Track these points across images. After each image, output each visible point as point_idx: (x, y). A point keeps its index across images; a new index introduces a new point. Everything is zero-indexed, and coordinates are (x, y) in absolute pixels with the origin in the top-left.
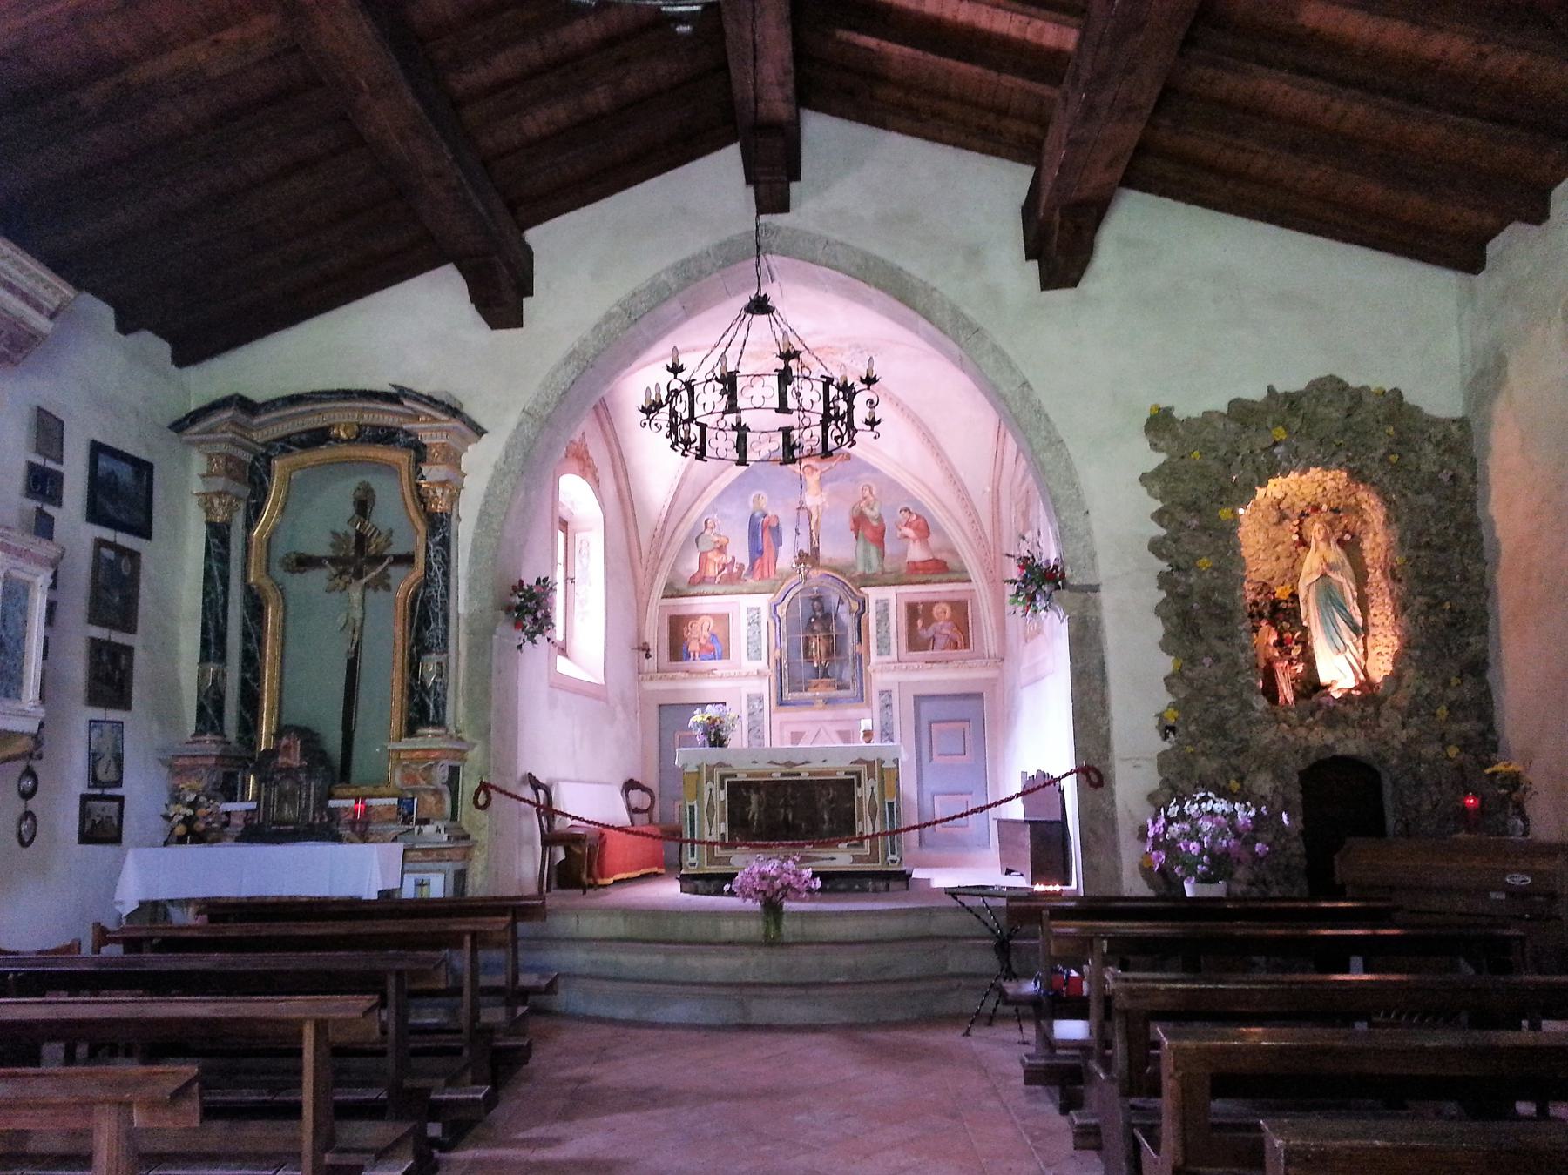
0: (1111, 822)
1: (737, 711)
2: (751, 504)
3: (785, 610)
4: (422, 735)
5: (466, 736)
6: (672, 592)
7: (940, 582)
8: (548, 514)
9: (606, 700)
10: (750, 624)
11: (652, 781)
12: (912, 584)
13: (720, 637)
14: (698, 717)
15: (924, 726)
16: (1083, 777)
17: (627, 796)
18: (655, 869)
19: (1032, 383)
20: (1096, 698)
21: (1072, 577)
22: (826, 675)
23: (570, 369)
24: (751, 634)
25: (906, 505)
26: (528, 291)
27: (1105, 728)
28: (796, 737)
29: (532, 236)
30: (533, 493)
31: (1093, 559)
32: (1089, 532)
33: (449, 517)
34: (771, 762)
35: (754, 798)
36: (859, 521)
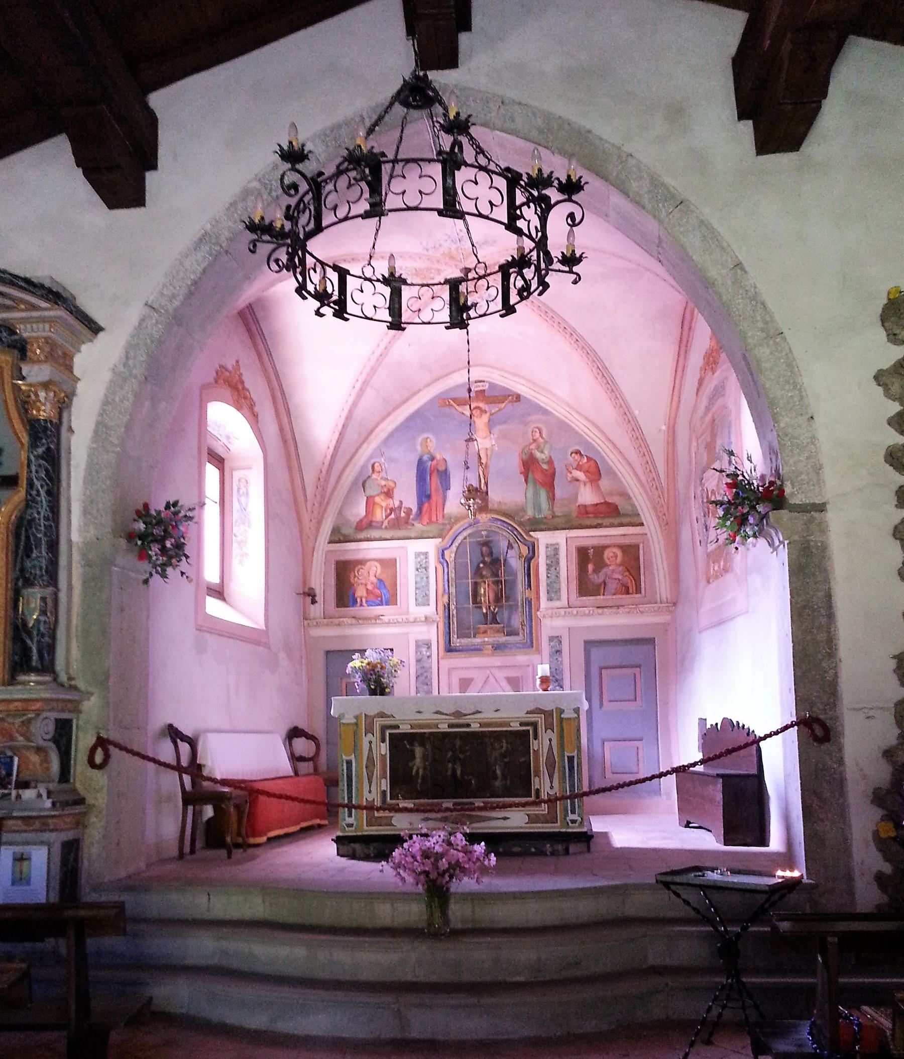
0: (840, 784)
1: (406, 654)
2: (419, 448)
3: (453, 555)
4: (23, 683)
5: (81, 684)
6: (339, 537)
7: (612, 526)
8: (194, 443)
9: (267, 645)
10: (417, 570)
11: (319, 730)
12: (582, 528)
13: (388, 582)
14: (357, 663)
15: (594, 670)
16: (805, 730)
17: (291, 745)
18: (318, 821)
19: (746, 265)
20: (821, 637)
21: (792, 494)
22: (494, 621)
23: (200, 255)
24: (419, 580)
25: (577, 448)
26: (153, 165)
27: (832, 672)
28: (465, 684)
29: (157, 100)
30: (163, 404)
31: (818, 474)
32: (813, 440)
33: (58, 427)
34: (438, 712)
35: (418, 751)
36: (529, 465)
